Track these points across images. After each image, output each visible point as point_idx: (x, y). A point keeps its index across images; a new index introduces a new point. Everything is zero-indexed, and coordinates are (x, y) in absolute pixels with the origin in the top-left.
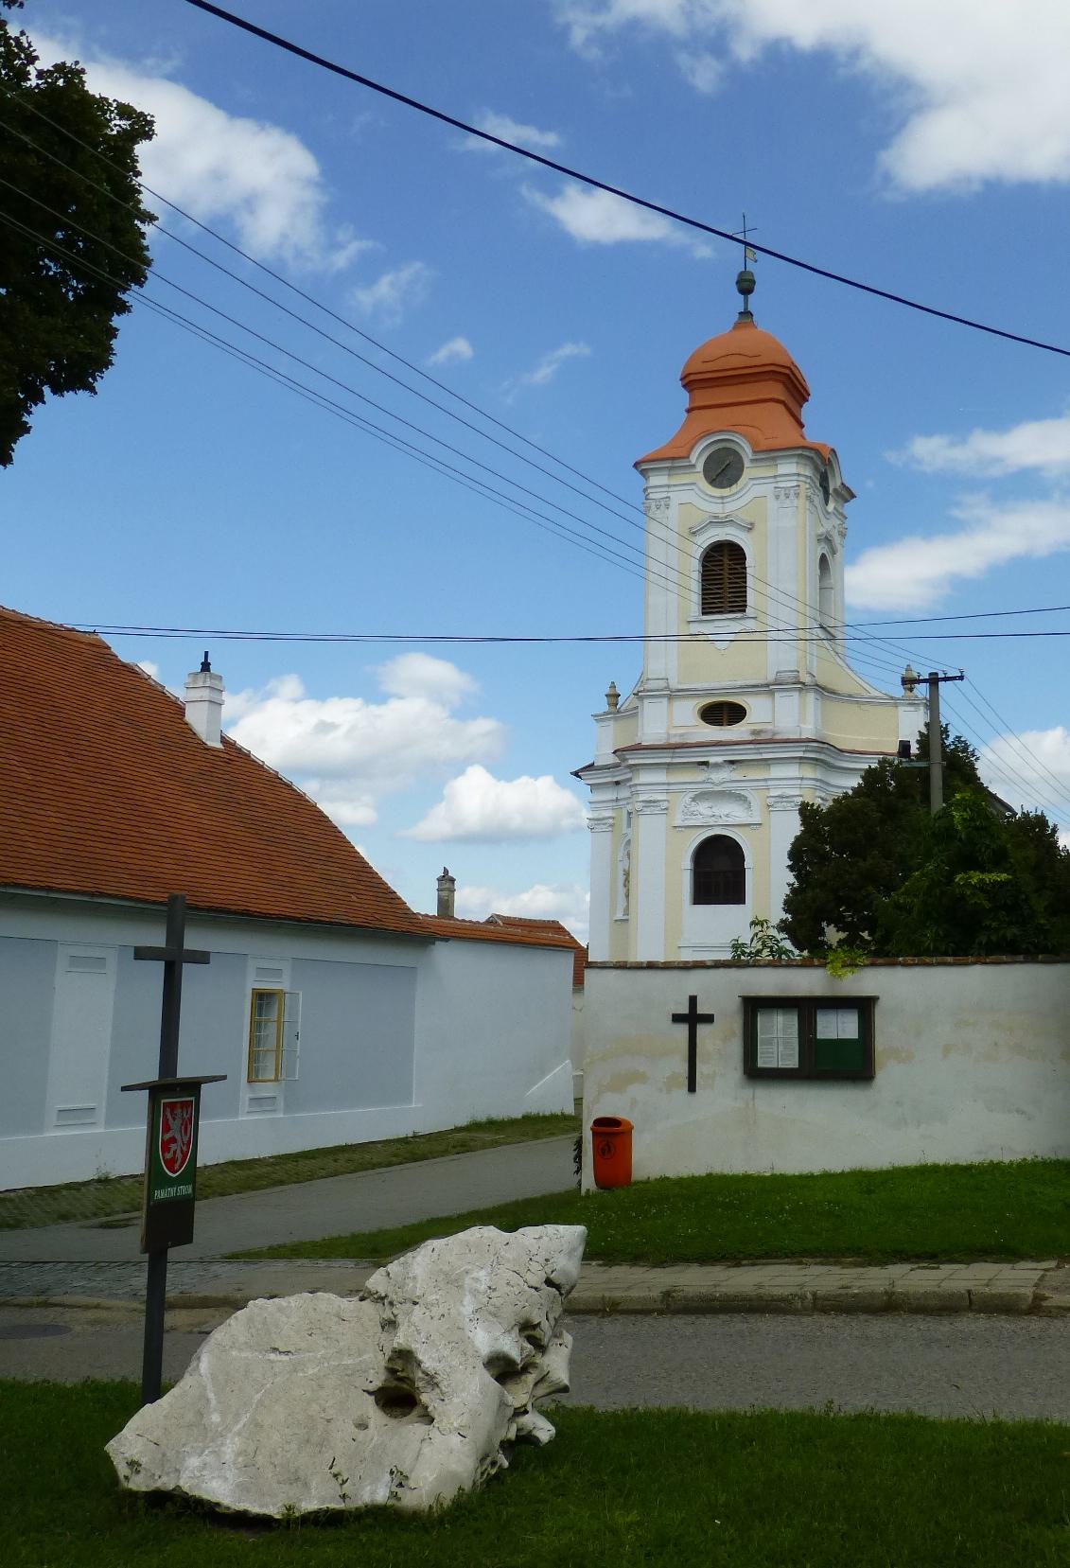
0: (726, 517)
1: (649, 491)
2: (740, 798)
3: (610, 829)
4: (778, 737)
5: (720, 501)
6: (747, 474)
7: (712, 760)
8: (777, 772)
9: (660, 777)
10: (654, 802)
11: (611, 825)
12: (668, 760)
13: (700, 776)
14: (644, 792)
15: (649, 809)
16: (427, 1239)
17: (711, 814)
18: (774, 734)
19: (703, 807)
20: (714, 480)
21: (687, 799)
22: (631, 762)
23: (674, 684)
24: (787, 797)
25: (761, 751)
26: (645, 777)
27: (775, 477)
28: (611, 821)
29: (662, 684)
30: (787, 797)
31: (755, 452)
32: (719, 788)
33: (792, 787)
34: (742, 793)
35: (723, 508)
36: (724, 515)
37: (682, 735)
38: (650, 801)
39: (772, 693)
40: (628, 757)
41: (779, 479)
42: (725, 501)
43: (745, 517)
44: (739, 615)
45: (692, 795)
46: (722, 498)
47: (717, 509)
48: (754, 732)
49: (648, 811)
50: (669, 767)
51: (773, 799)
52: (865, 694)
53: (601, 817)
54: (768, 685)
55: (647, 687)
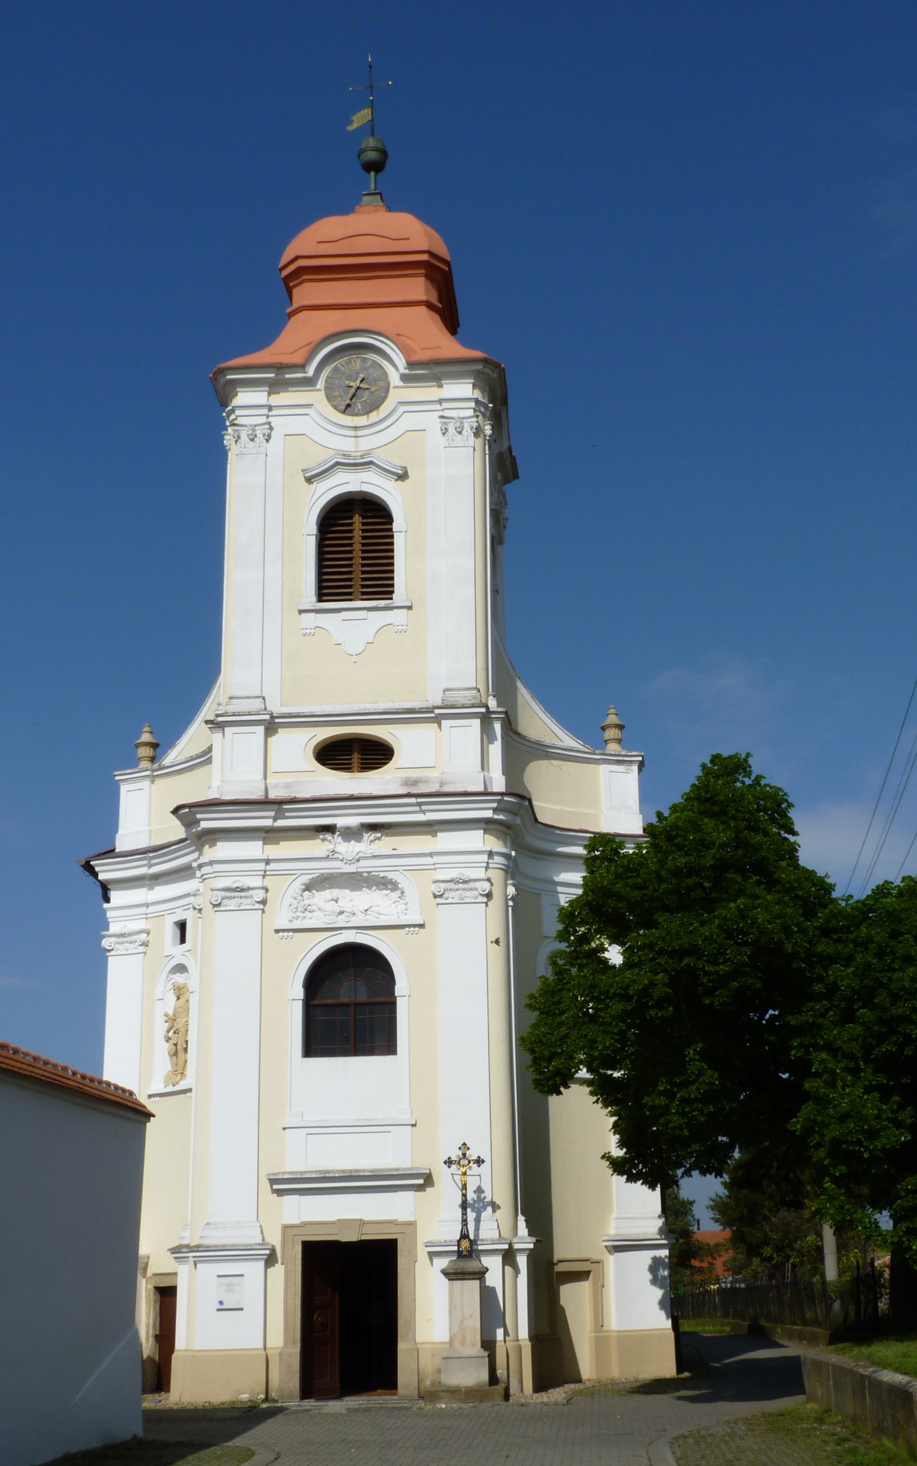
0: (362, 457)
1: (238, 412)
2: (386, 884)
3: (142, 949)
4: (448, 789)
5: (352, 433)
6: (394, 397)
7: (341, 822)
8: (446, 840)
9: (253, 849)
10: (242, 890)
11: (145, 944)
12: (268, 823)
13: (317, 847)
14: (217, 875)
15: (233, 902)
16: (530, 762)
17: (338, 910)
18: (442, 784)
19: (322, 898)
20: (348, 406)
21: (298, 885)
22: (204, 825)
23: (276, 707)
24: (465, 882)
25: (424, 808)
26: (224, 849)
27: (440, 401)
28: (144, 936)
29: (257, 705)
30: (465, 882)
31: (411, 365)
32: (352, 869)
33: (133, 918)
34: (390, 875)
35: (357, 444)
36: (359, 454)
37: (287, 786)
38: (235, 890)
39: (438, 720)
40: (199, 816)
41: (445, 405)
42: (360, 433)
43: (393, 459)
44: (382, 603)
45: (305, 879)
46: (356, 428)
47: (347, 445)
48: (407, 782)
49: (232, 904)
50: (269, 835)
51: (443, 885)
52: (559, 744)
53: (125, 931)
54: (430, 710)
55: (231, 709)
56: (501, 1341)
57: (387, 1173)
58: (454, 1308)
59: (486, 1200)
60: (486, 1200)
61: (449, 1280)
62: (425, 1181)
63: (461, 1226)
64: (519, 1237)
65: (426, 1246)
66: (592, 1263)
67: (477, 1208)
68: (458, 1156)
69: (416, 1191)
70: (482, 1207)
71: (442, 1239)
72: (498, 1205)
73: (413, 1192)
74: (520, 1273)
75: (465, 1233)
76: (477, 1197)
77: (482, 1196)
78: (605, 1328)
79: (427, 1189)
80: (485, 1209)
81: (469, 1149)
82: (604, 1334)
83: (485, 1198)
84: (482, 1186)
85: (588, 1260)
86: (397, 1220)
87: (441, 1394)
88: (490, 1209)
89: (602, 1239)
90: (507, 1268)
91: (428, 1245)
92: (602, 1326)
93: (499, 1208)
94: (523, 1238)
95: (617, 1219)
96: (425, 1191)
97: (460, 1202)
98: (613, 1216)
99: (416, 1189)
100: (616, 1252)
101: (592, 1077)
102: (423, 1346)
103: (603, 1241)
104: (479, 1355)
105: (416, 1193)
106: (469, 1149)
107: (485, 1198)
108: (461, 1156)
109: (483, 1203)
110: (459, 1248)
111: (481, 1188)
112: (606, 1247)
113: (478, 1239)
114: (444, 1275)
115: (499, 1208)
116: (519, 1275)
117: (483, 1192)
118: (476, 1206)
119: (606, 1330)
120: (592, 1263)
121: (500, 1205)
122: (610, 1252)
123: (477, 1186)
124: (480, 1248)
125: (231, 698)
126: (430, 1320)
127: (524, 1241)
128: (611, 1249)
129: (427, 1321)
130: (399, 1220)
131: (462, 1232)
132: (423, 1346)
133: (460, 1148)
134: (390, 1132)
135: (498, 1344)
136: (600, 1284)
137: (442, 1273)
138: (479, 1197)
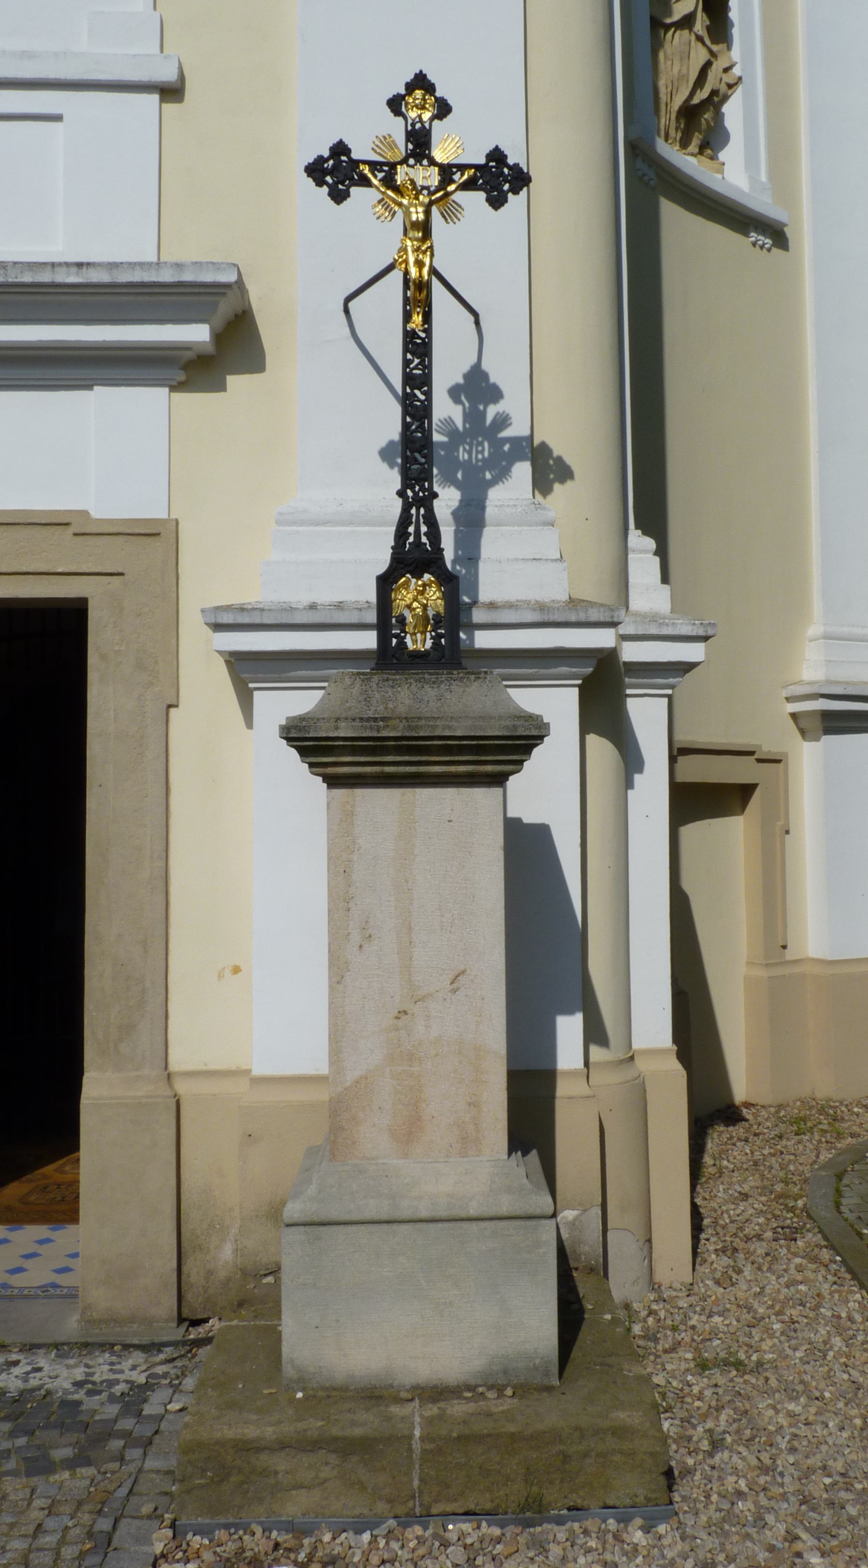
56: (572, 1074)
57: (27, 278)
58: (356, 937)
59: (505, 434)
60: (505, 434)
61: (332, 781)
62: (218, 337)
63: (398, 503)
64: (637, 614)
65: (218, 627)
66: (759, 761)
67: (467, 466)
68: (387, 141)
69: (173, 388)
70: (488, 464)
71: (300, 597)
72: (559, 460)
73: (163, 392)
74: (640, 769)
75: (418, 543)
76: (466, 417)
77: (492, 411)
78: (789, 955)
79: (232, 380)
80: (502, 474)
81: (443, 109)
82: (787, 971)
83: (503, 421)
84: (485, 366)
85: (751, 753)
86: (85, 514)
87: (280, 1463)
88: (523, 471)
89: (785, 693)
90: (592, 739)
91: (227, 618)
92: (784, 947)
93: (565, 473)
94: (654, 618)
95: (827, 637)
96: (221, 387)
97: (394, 432)
98: (814, 630)
99: (181, 376)
100: (828, 731)
101: (443, 615)
102: (204, 1087)
103: (788, 699)
104: (506, 1205)
105: (182, 398)
106: (443, 109)
107: (503, 421)
108: (401, 145)
109: (497, 444)
110: (384, 639)
111: (485, 376)
112: (794, 716)
113: (475, 602)
114: (303, 752)
115: (565, 473)
116: (637, 778)
117: (495, 394)
118: (463, 456)
119: (794, 958)
120: (759, 761)
121: (568, 460)
122: (803, 733)
123: (466, 368)
124: (484, 640)
125: (517, 1551)
126: (236, 970)
127: (665, 631)
128: (817, 723)
129: (220, 976)
130: (95, 514)
131: (401, 534)
132: (204, 1087)
133: (395, 105)
134: (58, 118)
135: (563, 1089)
136: (779, 823)
137: (289, 739)
138: (474, 417)
